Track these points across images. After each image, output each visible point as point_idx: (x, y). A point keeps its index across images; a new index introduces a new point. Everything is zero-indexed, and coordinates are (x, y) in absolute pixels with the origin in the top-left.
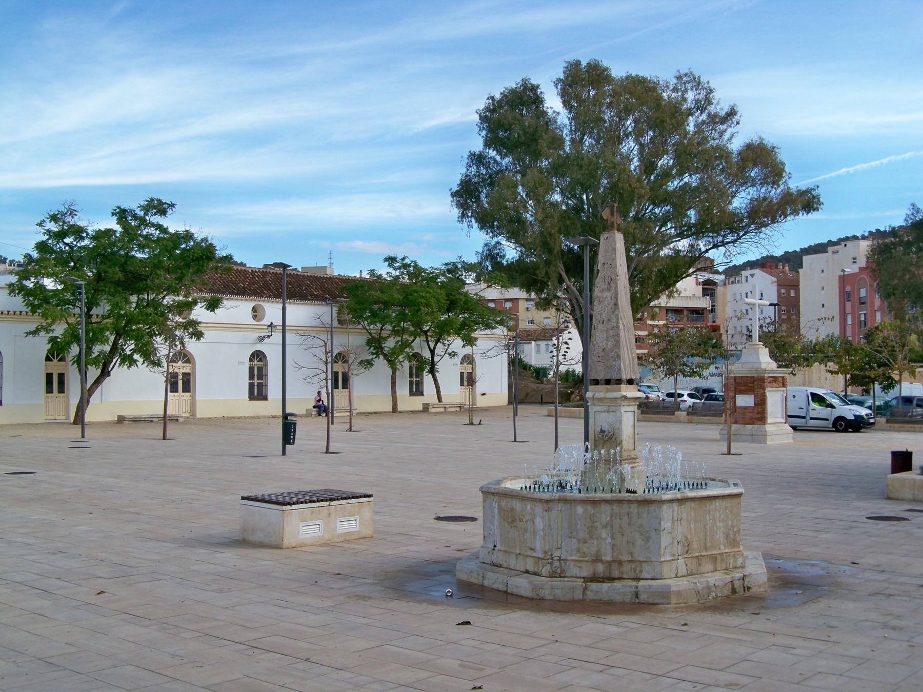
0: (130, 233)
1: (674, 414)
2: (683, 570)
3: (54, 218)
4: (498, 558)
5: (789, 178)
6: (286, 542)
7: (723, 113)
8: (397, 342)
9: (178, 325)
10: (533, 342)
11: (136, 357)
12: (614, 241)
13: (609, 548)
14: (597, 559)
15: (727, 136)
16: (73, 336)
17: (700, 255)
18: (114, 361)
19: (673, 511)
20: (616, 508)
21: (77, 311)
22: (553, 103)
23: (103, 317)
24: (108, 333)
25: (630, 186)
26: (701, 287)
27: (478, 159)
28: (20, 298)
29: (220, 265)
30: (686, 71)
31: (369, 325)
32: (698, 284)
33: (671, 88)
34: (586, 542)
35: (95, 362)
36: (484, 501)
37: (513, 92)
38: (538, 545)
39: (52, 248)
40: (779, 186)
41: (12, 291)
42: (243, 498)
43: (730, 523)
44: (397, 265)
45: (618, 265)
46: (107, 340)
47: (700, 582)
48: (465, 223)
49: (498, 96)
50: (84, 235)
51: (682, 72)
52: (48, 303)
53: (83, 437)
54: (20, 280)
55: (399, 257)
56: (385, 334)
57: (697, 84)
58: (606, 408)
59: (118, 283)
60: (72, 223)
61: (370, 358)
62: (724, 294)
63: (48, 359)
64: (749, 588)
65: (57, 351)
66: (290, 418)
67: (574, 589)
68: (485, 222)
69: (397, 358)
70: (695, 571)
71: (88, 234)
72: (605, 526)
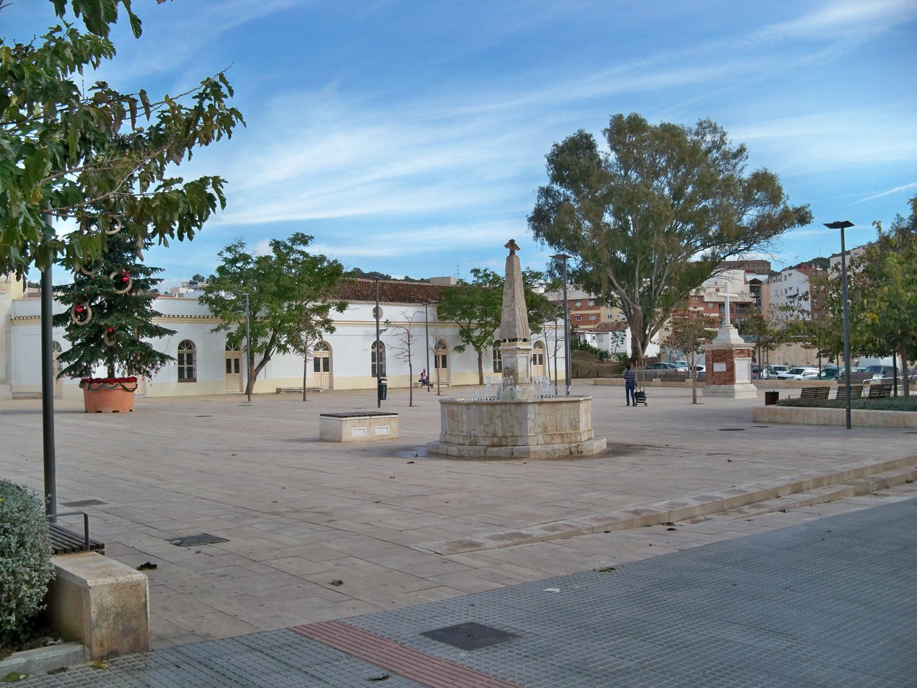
0: (282, 259)
1: (684, 381)
2: (541, 441)
3: (229, 249)
4: (447, 439)
5: (788, 199)
6: (344, 439)
7: (734, 150)
8: (482, 332)
9: (318, 323)
10: (610, 333)
11: (289, 346)
12: (513, 261)
13: (500, 429)
14: (494, 435)
15: (738, 167)
16: (242, 332)
17: (719, 260)
18: (273, 350)
19: (535, 409)
20: (503, 407)
21: (245, 314)
22: (603, 148)
23: (266, 318)
24: (268, 330)
25: (659, 210)
26: (749, 285)
27: (546, 192)
28: (206, 306)
29: (347, 279)
30: (706, 119)
31: (460, 319)
32: (746, 282)
33: (693, 132)
34: (488, 426)
35: (260, 350)
36: (441, 408)
37: (572, 140)
38: (464, 430)
39: (228, 271)
40: (779, 205)
41: (201, 301)
42: (321, 415)
43: (573, 417)
44: (480, 275)
45: (515, 274)
46: (267, 334)
47: (549, 448)
48: (539, 241)
49: (560, 144)
50: (250, 261)
51: (703, 120)
52: (226, 309)
53: (249, 400)
54: (206, 294)
55: (482, 269)
56: (472, 326)
57: (714, 129)
58: (509, 355)
59: (274, 294)
60: (241, 252)
61: (462, 344)
62: (768, 291)
63: (227, 349)
64: (581, 452)
65: (233, 342)
66: (383, 382)
67: (480, 451)
68: (553, 240)
69: (482, 344)
70: (549, 442)
71: (252, 260)
72: (498, 417)
